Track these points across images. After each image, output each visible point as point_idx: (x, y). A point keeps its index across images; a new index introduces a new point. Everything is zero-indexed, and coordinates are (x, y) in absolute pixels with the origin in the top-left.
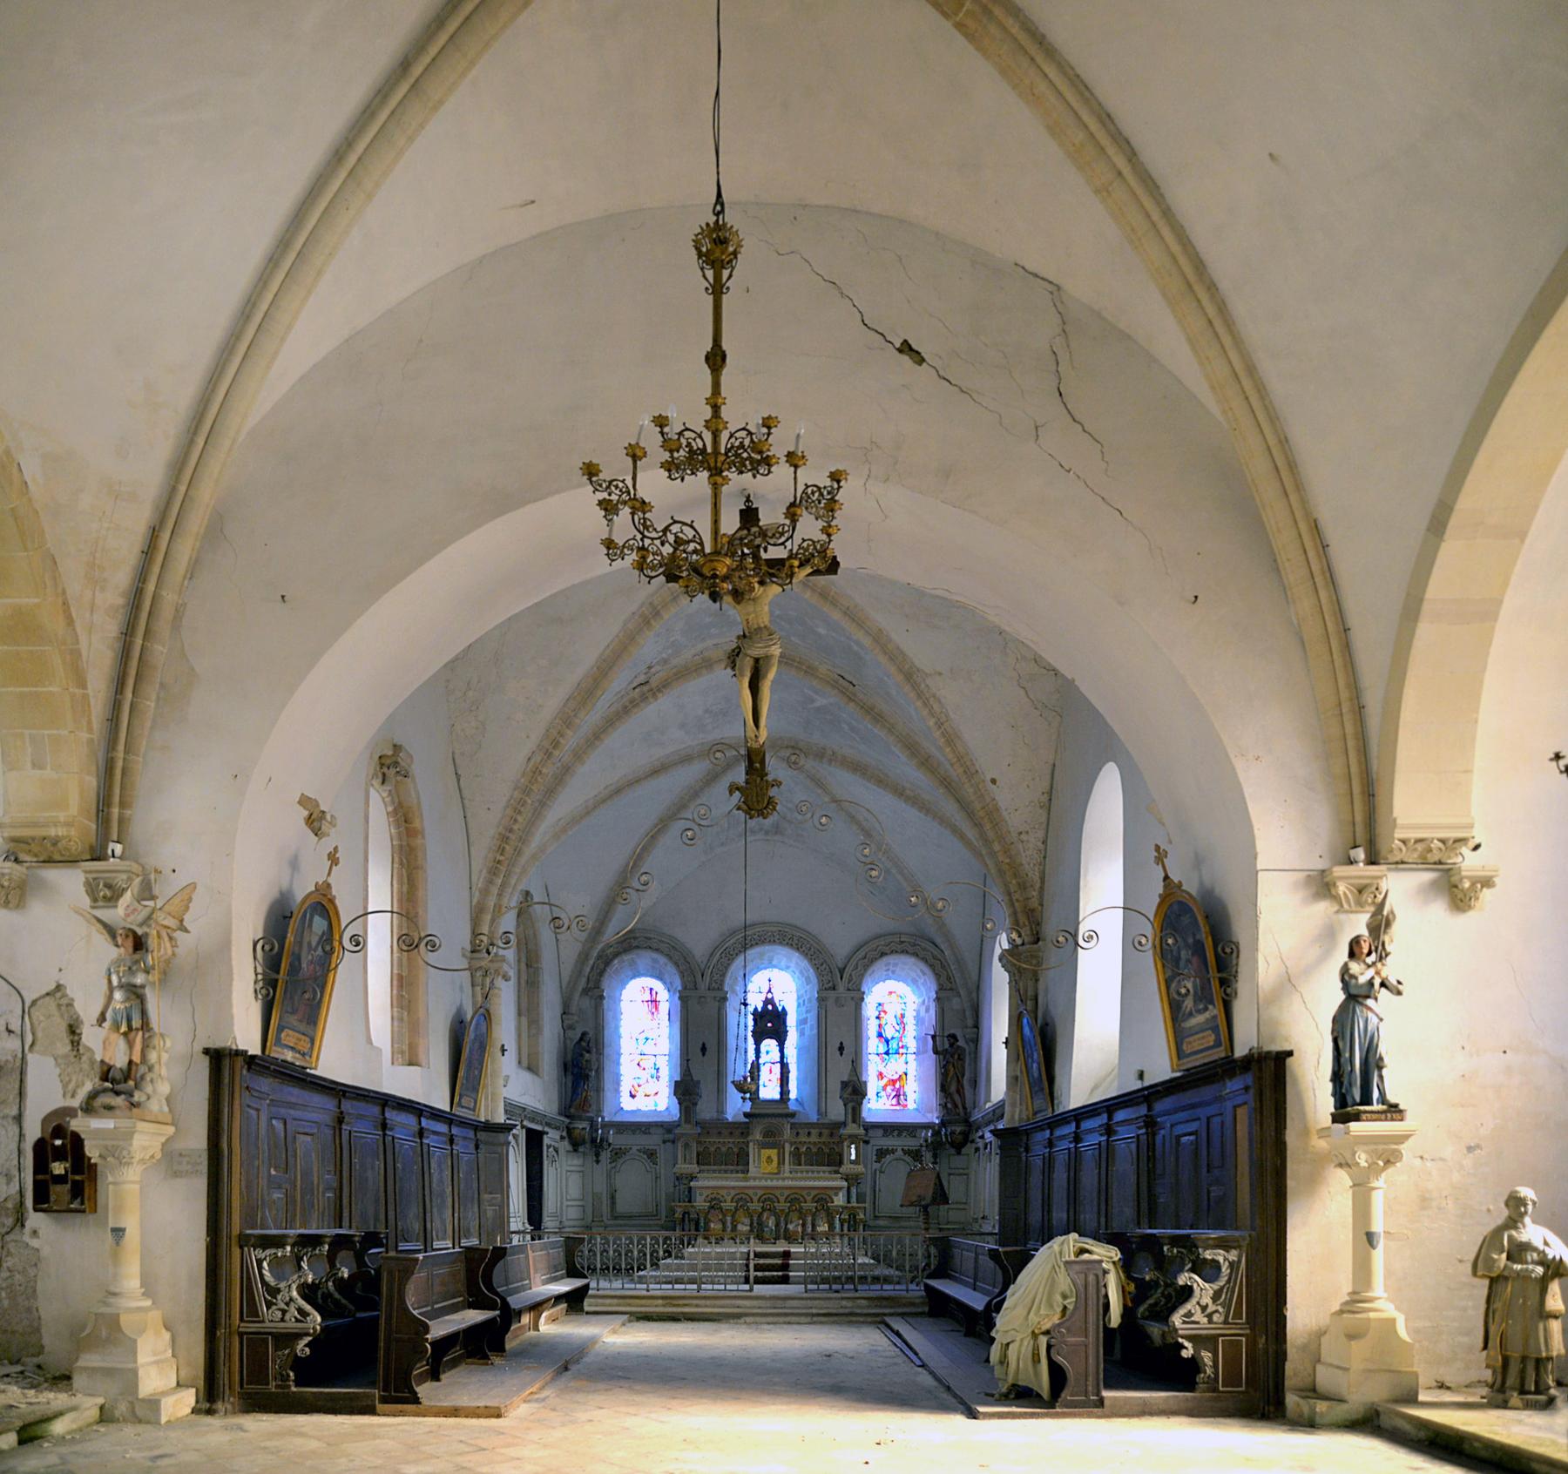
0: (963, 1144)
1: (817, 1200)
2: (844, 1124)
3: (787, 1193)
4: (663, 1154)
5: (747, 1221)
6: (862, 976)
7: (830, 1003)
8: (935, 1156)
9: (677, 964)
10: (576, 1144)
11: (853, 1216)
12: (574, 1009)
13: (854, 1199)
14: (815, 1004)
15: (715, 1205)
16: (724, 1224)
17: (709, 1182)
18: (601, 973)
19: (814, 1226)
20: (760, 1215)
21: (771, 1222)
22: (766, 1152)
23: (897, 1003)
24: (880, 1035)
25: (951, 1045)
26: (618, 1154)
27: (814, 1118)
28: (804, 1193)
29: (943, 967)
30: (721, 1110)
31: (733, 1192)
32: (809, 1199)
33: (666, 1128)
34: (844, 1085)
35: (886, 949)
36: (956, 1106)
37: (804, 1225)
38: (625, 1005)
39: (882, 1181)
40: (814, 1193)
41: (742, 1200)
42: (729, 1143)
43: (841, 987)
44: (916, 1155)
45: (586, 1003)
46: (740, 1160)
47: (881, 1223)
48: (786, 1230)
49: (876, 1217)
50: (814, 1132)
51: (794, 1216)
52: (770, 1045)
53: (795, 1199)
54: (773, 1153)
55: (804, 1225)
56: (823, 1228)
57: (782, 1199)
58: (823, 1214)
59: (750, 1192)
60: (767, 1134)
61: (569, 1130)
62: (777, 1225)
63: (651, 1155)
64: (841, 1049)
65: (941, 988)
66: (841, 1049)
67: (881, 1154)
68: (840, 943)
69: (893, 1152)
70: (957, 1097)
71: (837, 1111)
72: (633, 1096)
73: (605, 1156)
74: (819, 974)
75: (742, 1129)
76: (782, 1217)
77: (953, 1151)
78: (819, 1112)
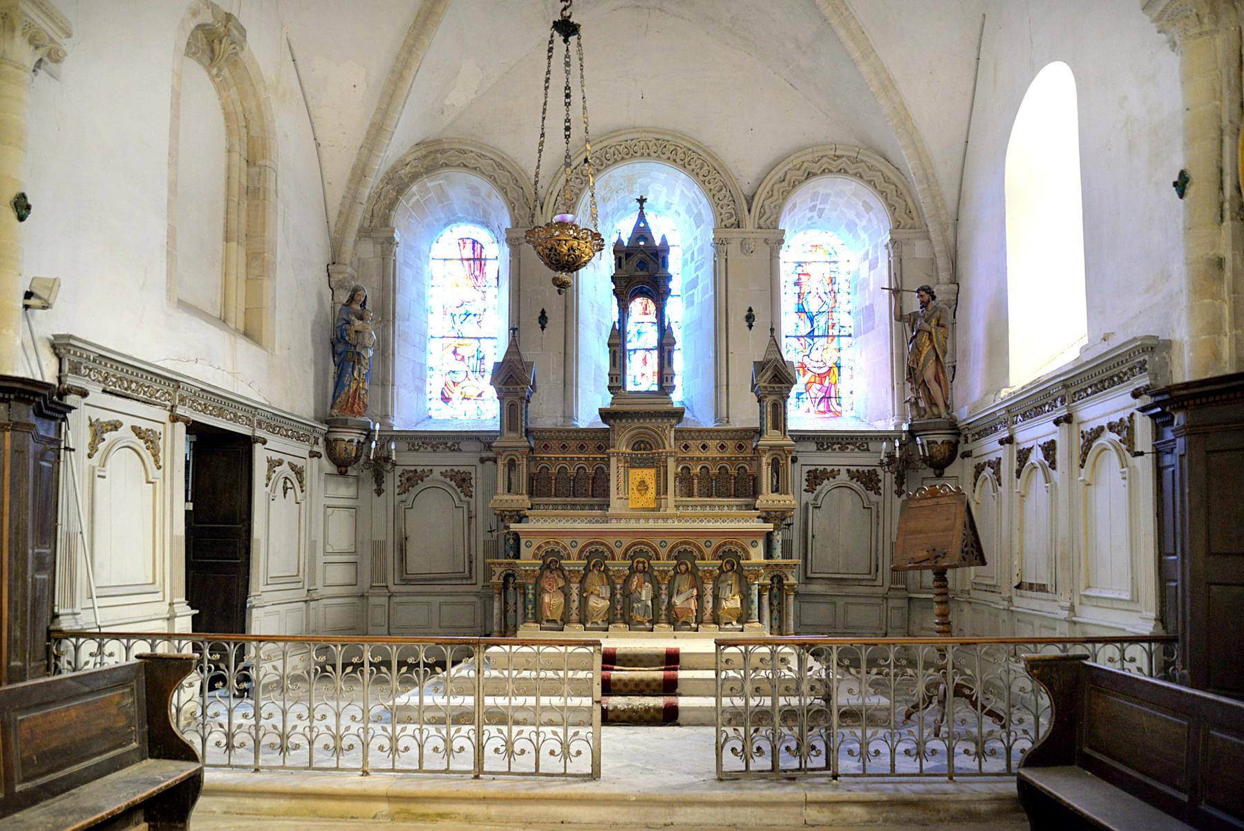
0: (950, 459)
1: (721, 554)
2: (759, 432)
3: (671, 542)
4: (479, 477)
5: (605, 591)
6: (779, 208)
7: (733, 248)
8: (900, 480)
9: (505, 193)
10: (341, 465)
11: (778, 579)
12: (347, 256)
13: (778, 551)
14: (710, 251)
15: (551, 562)
16: (567, 596)
17: (551, 524)
18: (392, 205)
19: (717, 599)
20: (627, 580)
21: (646, 593)
22: (637, 474)
23: (835, 259)
24: (801, 311)
25: (924, 305)
26: (412, 479)
27: (709, 423)
28: (701, 542)
29: (899, 195)
30: (569, 415)
31: (581, 542)
32: (708, 552)
33: (482, 440)
34: (760, 367)
35: (815, 168)
36: (932, 402)
37: (700, 598)
38: (434, 269)
39: (817, 522)
40: (716, 542)
41: (596, 556)
42: (576, 461)
43: (750, 222)
44: (869, 480)
45: (368, 250)
46: (592, 489)
47: (816, 588)
48: (671, 606)
49: (808, 580)
50: (712, 444)
51: (684, 582)
52: (639, 307)
53: (685, 554)
54: (648, 475)
55: (700, 598)
56: (732, 602)
57: (663, 552)
58: (732, 579)
59: (611, 541)
60: (638, 445)
61: (330, 445)
62: (655, 598)
63: (463, 481)
64: (750, 318)
65: (897, 226)
66: (750, 318)
67: (815, 478)
68: (746, 160)
69: (834, 474)
70: (935, 388)
71: (746, 413)
72: (446, 399)
73: (391, 482)
74: (716, 202)
75: (598, 440)
76: (663, 585)
77: (930, 472)
78: (717, 418)
